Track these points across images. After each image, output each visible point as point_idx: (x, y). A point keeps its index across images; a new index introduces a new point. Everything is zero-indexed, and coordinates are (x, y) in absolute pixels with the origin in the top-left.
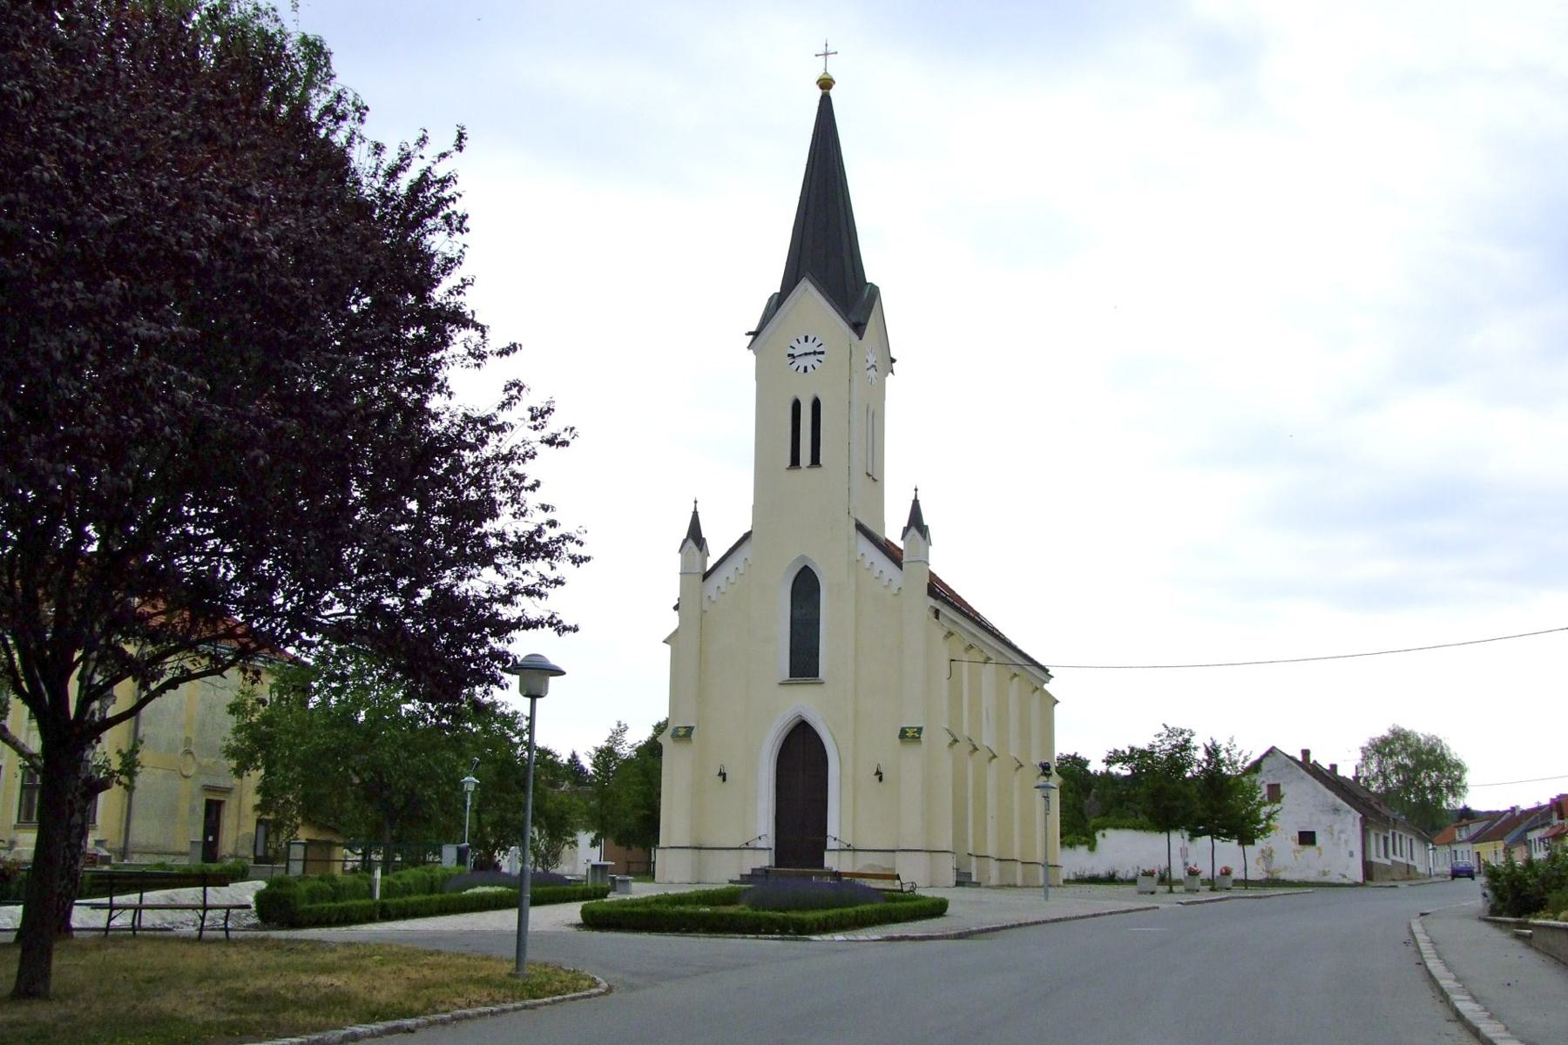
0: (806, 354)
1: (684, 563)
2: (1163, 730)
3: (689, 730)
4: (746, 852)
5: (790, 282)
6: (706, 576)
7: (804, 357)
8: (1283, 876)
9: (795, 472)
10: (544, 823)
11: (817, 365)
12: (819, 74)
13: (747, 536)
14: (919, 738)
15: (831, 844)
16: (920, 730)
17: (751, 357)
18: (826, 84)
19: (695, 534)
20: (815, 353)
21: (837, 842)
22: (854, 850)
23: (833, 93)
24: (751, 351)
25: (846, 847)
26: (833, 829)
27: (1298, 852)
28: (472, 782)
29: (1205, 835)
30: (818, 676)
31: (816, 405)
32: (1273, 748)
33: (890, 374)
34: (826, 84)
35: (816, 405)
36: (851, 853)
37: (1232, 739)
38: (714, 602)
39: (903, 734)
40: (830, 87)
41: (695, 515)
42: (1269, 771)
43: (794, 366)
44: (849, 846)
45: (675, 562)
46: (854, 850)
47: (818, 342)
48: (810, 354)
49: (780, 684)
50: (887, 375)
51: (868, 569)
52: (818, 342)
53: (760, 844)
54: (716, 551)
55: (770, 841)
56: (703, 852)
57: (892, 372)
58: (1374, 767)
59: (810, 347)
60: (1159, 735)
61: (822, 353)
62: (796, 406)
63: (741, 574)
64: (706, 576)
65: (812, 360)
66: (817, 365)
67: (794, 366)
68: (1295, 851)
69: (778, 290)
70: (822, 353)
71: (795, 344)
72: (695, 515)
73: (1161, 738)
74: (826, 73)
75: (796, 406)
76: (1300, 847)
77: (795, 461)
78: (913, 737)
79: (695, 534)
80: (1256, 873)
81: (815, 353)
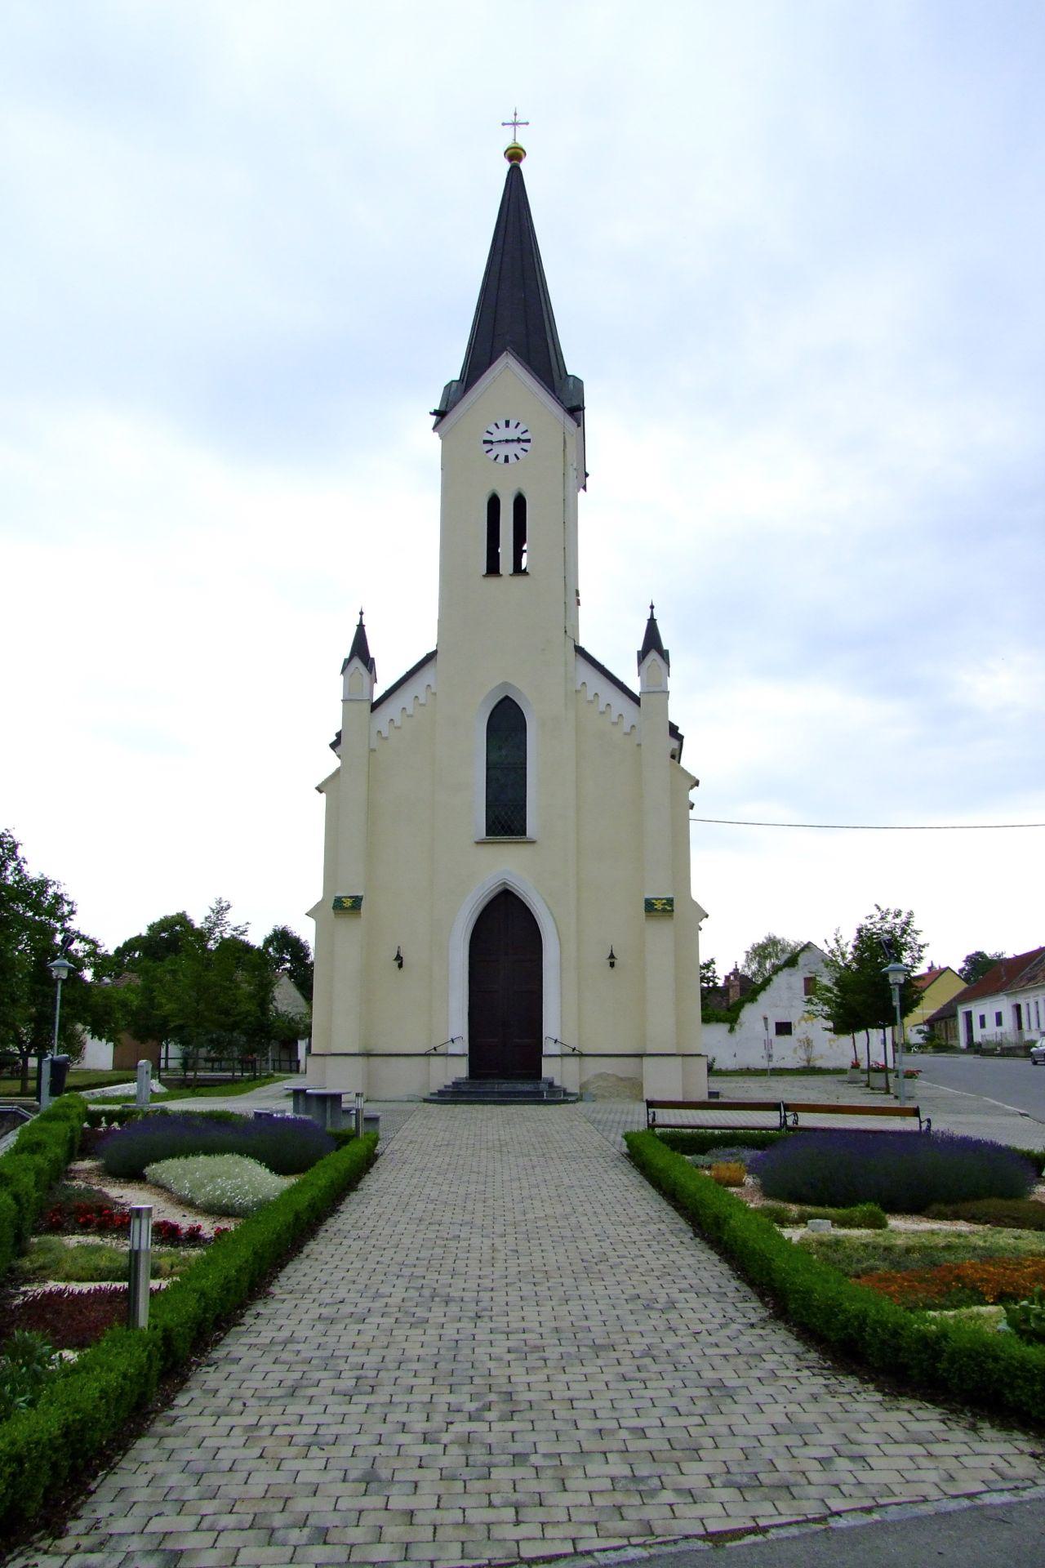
0: (507, 441)
1: (348, 688)
2: (875, 911)
3: (357, 902)
4: (433, 1059)
5: (477, 363)
6: (375, 706)
7: (503, 444)
8: (819, 1063)
9: (493, 581)
10: (89, 1019)
11: (521, 454)
12: (508, 143)
13: (430, 657)
14: (673, 911)
15: (548, 1047)
16: (670, 902)
17: (434, 442)
18: (515, 155)
19: (360, 649)
20: (519, 440)
21: (558, 1045)
22: (582, 1055)
23: (523, 166)
24: (437, 434)
25: (570, 1051)
26: (552, 1025)
27: (833, 1040)
28: (65, 966)
29: (723, 1022)
30: (525, 834)
31: (520, 503)
32: (809, 943)
33: (582, 490)
34: (515, 155)
35: (520, 503)
36: (578, 1058)
37: (838, 930)
38: (386, 738)
39: (649, 906)
40: (520, 159)
41: (361, 628)
42: (806, 965)
43: (492, 455)
44: (574, 1049)
45: (336, 686)
46: (582, 1055)
47: (522, 428)
48: (513, 441)
49: (477, 843)
50: (579, 491)
51: (591, 702)
52: (522, 428)
53: (453, 1049)
54: (386, 678)
55: (462, 1047)
56: (372, 1059)
57: (585, 488)
58: (754, 966)
59: (512, 433)
60: (871, 917)
61: (528, 441)
62: (494, 504)
63: (421, 705)
64: (375, 706)
65: (514, 448)
66: (521, 454)
67: (492, 455)
68: (830, 1040)
69: (457, 378)
70: (528, 441)
71: (492, 429)
72: (361, 628)
73: (872, 921)
74: (515, 143)
75: (494, 504)
76: (835, 1037)
77: (493, 568)
78: (664, 910)
79: (360, 649)
80: (794, 1060)
81: (519, 440)
